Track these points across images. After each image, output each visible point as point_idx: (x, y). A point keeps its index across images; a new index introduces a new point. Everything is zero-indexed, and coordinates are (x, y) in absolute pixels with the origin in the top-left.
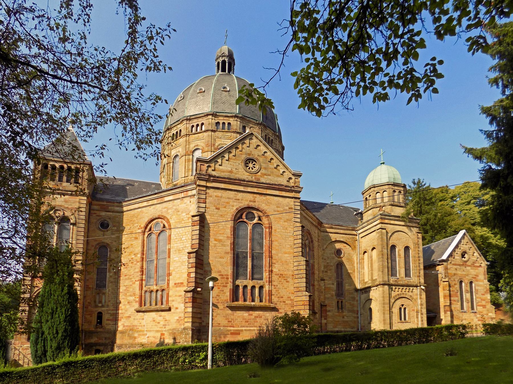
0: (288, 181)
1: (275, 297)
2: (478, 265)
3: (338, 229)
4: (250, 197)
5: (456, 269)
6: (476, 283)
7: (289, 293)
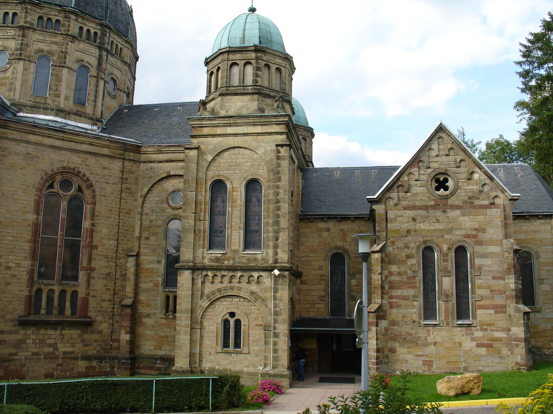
2: (486, 202)
5: (414, 220)
6: (478, 249)
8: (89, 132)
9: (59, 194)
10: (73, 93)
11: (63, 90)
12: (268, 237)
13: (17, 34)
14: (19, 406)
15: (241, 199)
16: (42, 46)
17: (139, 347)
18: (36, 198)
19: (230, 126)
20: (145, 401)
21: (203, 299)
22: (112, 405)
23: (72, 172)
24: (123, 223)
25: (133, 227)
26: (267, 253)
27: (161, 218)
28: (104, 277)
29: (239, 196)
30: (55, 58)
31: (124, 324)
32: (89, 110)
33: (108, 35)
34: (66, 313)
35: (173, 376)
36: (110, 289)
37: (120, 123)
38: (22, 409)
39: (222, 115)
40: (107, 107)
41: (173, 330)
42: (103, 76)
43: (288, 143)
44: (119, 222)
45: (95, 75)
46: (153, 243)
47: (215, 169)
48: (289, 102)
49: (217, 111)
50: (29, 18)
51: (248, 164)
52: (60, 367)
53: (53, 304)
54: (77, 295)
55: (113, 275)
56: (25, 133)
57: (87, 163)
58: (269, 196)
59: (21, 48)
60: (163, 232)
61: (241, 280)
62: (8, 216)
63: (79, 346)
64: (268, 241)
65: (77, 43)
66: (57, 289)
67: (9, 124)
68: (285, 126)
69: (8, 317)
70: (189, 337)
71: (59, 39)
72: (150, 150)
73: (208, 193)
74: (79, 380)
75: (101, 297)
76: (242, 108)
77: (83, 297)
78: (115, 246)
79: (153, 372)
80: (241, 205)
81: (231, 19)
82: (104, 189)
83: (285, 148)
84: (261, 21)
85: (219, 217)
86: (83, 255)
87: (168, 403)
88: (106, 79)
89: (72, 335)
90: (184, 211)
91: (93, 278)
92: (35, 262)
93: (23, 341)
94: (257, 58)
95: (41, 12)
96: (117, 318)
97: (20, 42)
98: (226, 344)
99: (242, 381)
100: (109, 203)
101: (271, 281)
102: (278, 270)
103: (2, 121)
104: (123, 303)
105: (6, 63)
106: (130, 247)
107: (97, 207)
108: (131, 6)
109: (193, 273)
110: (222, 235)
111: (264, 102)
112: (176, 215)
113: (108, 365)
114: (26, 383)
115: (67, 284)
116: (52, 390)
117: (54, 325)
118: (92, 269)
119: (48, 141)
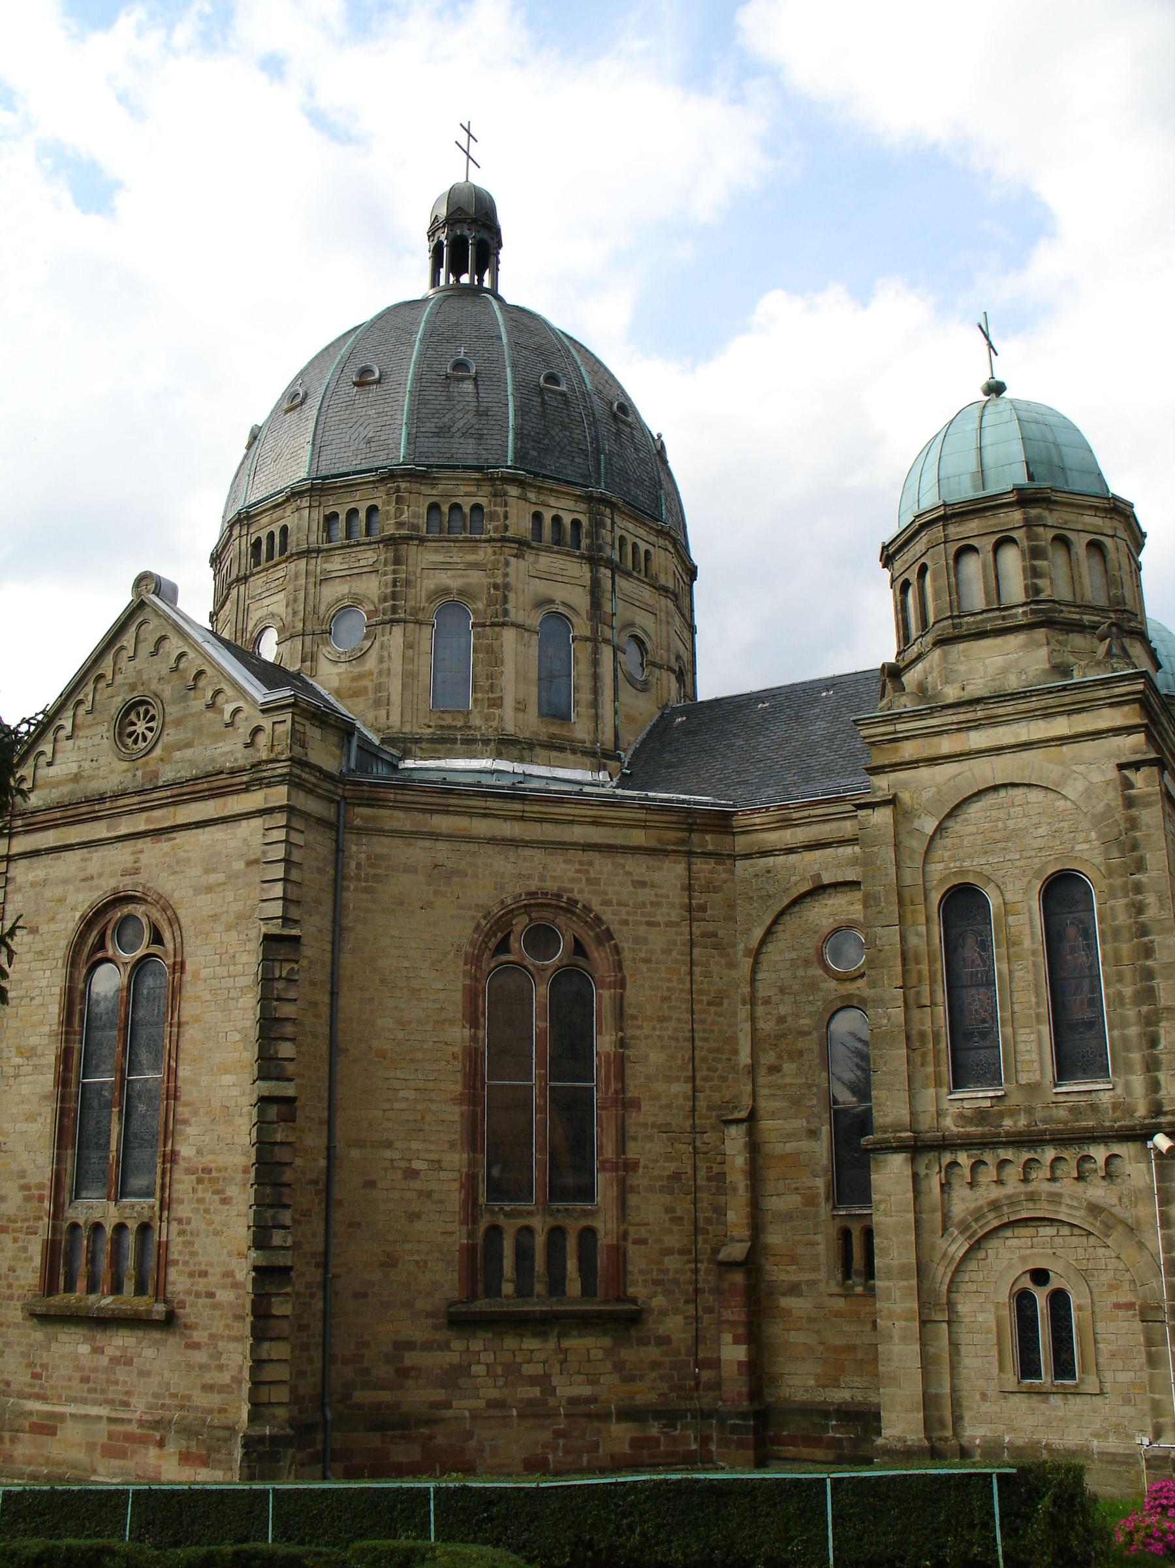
0: (247, 746)
1: (180, 1273)
3: (826, 819)
4: (122, 855)
7: (230, 1254)
8: (587, 789)
9: (525, 967)
10: (534, 691)
11: (510, 686)
12: (1125, 1039)
13: (382, 558)
14: (472, 1550)
15: (1033, 933)
16: (445, 579)
17: (774, 1379)
18: (468, 982)
19: (976, 728)
20: (803, 1542)
21: (951, 1234)
22: (712, 1550)
23: (554, 902)
24: (704, 1031)
25: (732, 1041)
26: (1128, 1087)
27: (808, 1008)
28: (663, 1187)
29: (1027, 927)
30: (480, 606)
31: (728, 1315)
32: (581, 729)
33: (608, 522)
34: (567, 1289)
35: (882, 1467)
36: (681, 1218)
37: (668, 757)
38: (482, 1557)
39: (950, 701)
40: (627, 716)
41: (868, 1328)
42: (608, 633)
43: (1153, 755)
44: (693, 1030)
45: (587, 633)
46: (794, 1081)
47: (947, 854)
48: (1141, 635)
49: (934, 689)
50: (406, 515)
51: (1042, 831)
52: (561, 1442)
53: (532, 1269)
54: (596, 1241)
55: (687, 1180)
56: (424, 811)
57: (592, 875)
58: (1114, 918)
59: (393, 592)
60: (815, 1047)
61: (1058, 1173)
62: (400, 1035)
63: (610, 1380)
64: (1127, 1049)
65: (530, 557)
66: (541, 1225)
67: (382, 793)
68: (1137, 706)
69: (420, 1304)
70: (917, 1347)
71: (485, 554)
72: (757, 821)
73: (936, 927)
74: (620, 1480)
75: (660, 1241)
76: (1004, 671)
77: (613, 1245)
78: (686, 1098)
79: (819, 1454)
80: (1034, 953)
81: (938, 424)
82: (645, 941)
83: (1145, 770)
84: (1023, 415)
85: (973, 991)
86: (602, 1127)
87: (874, 1548)
88: (616, 641)
89: (588, 1350)
90: (873, 985)
91: (633, 1189)
92: (479, 1156)
93: (462, 1370)
94: (1028, 524)
95: (434, 492)
96: (709, 1299)
97: (390, 577)
98: (1029, 1368)
99: (1092, 1483)
100: (660, 979)
101: (1149, 1169)
102: (1167, 1134)
103: (365, 788)
104: (722, 1256)
105: (362, 636)
106: (728, 1097)
107: (630, 993)
108: (659, 436)
109: (913, 1161)
110: (988, 1043)
111: (1066, 646)
112: (850, 996)
113: (691, 1433)
114: (481, 1485)
115: (567, 1210)
116: (548, 1507)
117: (541, 1324)
118: (630, 1167)
119: (483, 827)
